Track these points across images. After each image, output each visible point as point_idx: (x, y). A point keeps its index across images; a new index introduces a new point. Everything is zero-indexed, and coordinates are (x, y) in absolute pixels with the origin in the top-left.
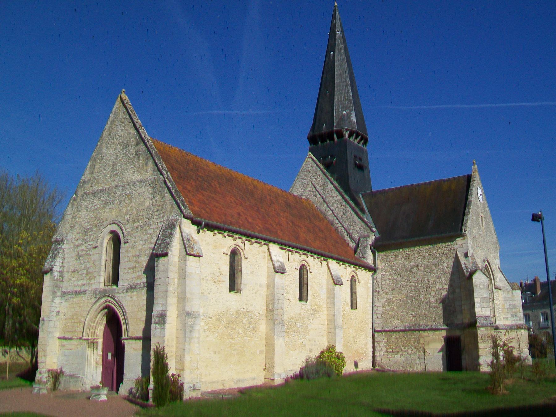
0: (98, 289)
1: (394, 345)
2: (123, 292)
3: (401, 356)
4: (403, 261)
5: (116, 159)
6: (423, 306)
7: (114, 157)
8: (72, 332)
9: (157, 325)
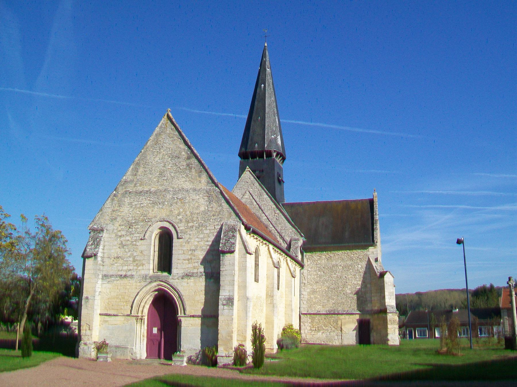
0: (148, 274)
2: (178, 279)
3: (322, 333)
5: (164, 167)
8: (117, 310)
9: (224, 306)
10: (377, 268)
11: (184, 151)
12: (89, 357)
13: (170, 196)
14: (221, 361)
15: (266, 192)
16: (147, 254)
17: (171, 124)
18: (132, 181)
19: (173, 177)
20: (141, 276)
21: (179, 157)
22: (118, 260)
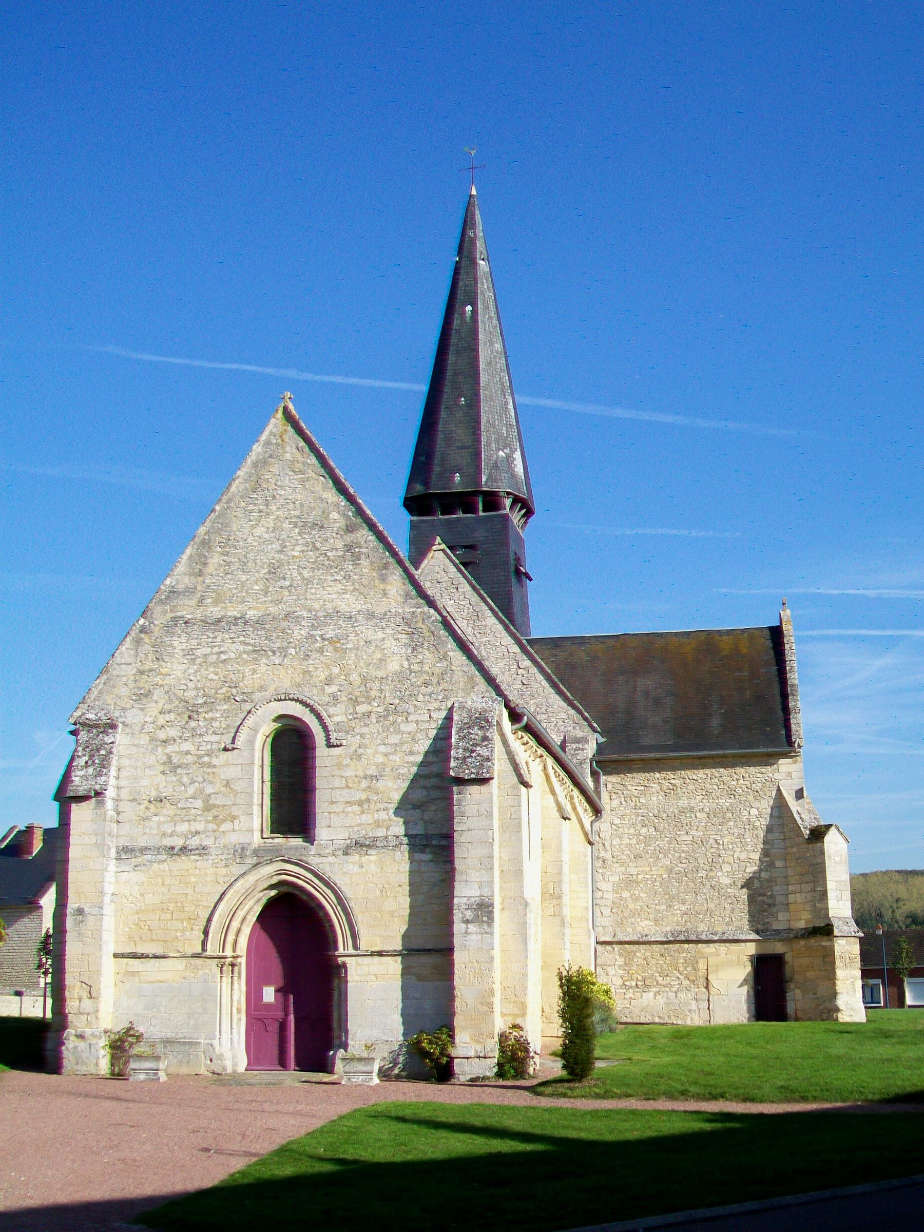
0: (249, 844)
1: (640, 972)
2: (334, 855)
3: (655, 995)
4: (661, 797)
6: (704, 894)
7: (276, 546)
8: (164, 941)
10: (802, 816)
11: (336, 510)
12: (93, 1071)
13: (303, 632)
14: (464, 1070)
15: (491, 609)
16: (242, 789)
17: (296, 436)
18: (190, 591)
19: (308, 581)
20: (228, 849)
21: (322, 527)
22: (161, 807)
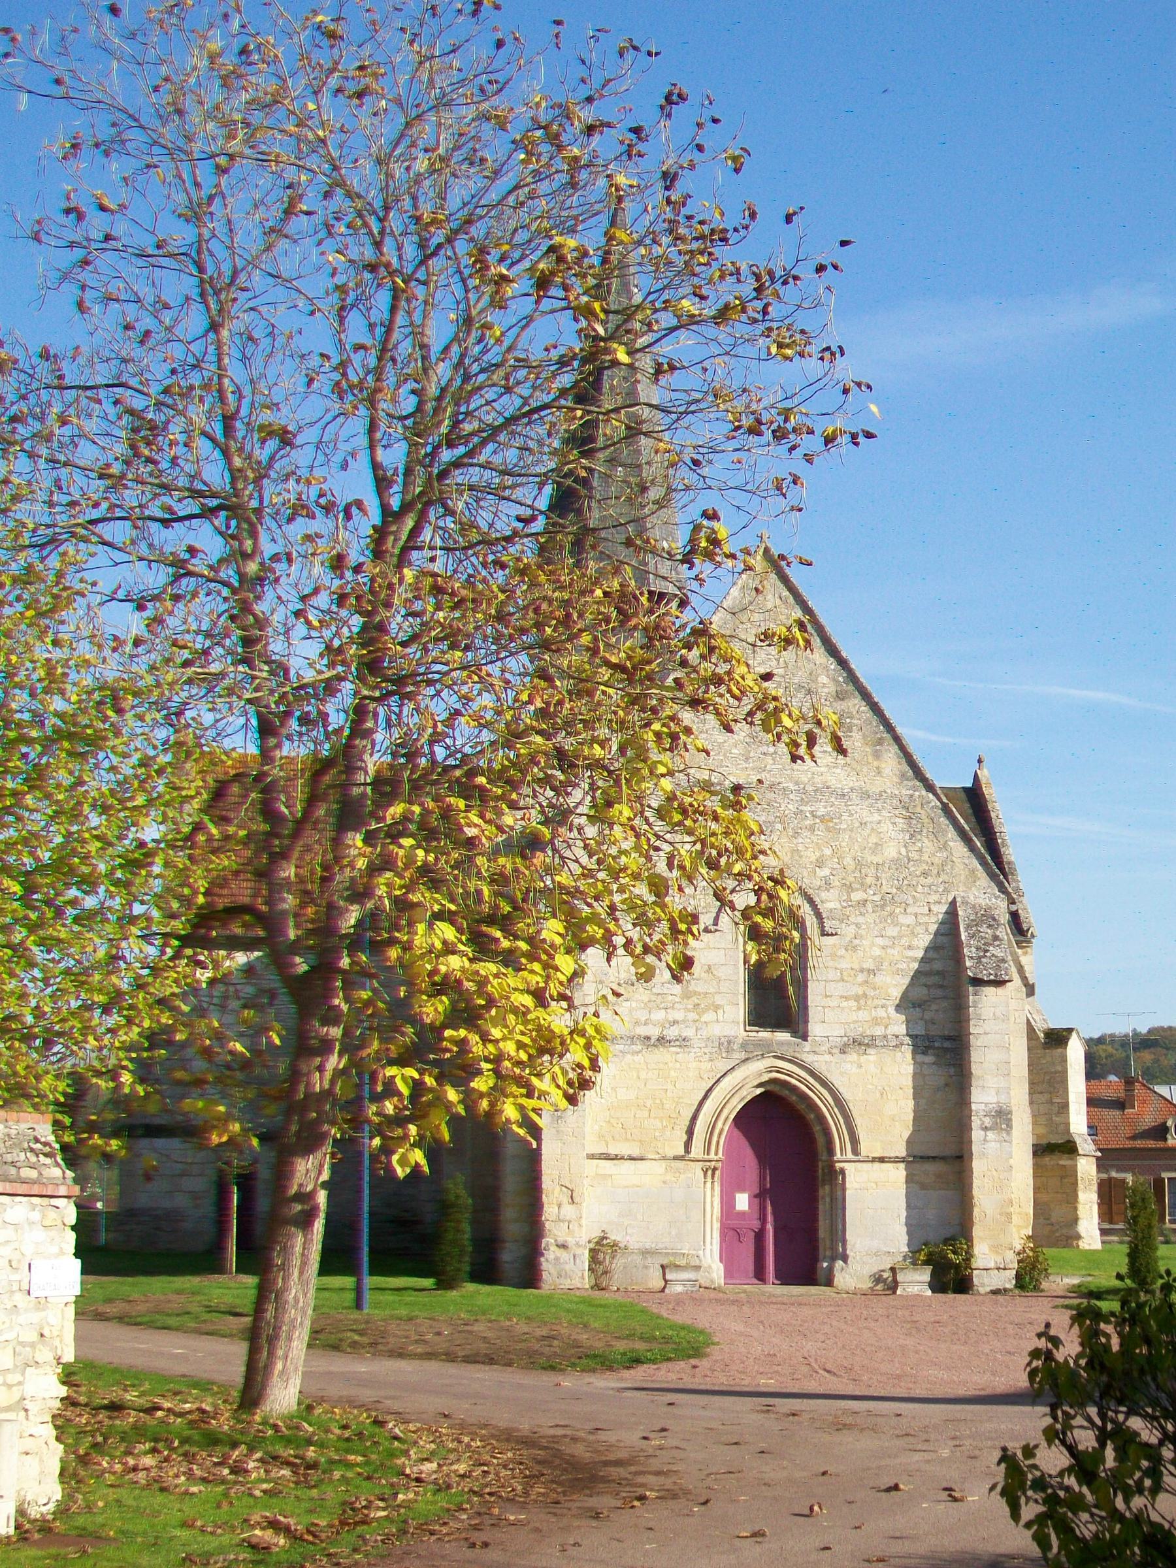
14: (984, 1281)
